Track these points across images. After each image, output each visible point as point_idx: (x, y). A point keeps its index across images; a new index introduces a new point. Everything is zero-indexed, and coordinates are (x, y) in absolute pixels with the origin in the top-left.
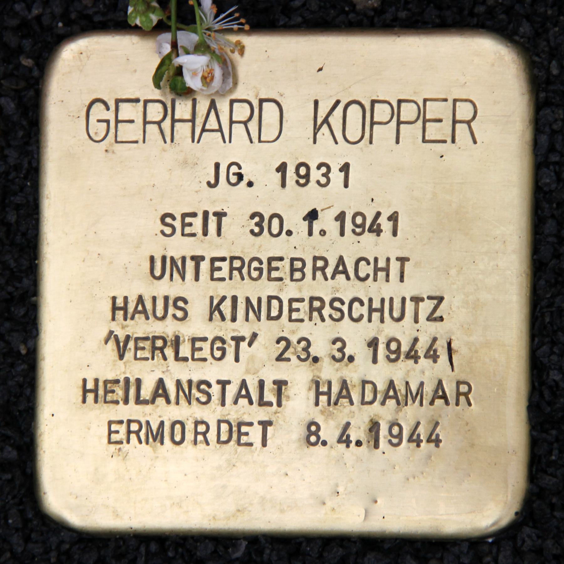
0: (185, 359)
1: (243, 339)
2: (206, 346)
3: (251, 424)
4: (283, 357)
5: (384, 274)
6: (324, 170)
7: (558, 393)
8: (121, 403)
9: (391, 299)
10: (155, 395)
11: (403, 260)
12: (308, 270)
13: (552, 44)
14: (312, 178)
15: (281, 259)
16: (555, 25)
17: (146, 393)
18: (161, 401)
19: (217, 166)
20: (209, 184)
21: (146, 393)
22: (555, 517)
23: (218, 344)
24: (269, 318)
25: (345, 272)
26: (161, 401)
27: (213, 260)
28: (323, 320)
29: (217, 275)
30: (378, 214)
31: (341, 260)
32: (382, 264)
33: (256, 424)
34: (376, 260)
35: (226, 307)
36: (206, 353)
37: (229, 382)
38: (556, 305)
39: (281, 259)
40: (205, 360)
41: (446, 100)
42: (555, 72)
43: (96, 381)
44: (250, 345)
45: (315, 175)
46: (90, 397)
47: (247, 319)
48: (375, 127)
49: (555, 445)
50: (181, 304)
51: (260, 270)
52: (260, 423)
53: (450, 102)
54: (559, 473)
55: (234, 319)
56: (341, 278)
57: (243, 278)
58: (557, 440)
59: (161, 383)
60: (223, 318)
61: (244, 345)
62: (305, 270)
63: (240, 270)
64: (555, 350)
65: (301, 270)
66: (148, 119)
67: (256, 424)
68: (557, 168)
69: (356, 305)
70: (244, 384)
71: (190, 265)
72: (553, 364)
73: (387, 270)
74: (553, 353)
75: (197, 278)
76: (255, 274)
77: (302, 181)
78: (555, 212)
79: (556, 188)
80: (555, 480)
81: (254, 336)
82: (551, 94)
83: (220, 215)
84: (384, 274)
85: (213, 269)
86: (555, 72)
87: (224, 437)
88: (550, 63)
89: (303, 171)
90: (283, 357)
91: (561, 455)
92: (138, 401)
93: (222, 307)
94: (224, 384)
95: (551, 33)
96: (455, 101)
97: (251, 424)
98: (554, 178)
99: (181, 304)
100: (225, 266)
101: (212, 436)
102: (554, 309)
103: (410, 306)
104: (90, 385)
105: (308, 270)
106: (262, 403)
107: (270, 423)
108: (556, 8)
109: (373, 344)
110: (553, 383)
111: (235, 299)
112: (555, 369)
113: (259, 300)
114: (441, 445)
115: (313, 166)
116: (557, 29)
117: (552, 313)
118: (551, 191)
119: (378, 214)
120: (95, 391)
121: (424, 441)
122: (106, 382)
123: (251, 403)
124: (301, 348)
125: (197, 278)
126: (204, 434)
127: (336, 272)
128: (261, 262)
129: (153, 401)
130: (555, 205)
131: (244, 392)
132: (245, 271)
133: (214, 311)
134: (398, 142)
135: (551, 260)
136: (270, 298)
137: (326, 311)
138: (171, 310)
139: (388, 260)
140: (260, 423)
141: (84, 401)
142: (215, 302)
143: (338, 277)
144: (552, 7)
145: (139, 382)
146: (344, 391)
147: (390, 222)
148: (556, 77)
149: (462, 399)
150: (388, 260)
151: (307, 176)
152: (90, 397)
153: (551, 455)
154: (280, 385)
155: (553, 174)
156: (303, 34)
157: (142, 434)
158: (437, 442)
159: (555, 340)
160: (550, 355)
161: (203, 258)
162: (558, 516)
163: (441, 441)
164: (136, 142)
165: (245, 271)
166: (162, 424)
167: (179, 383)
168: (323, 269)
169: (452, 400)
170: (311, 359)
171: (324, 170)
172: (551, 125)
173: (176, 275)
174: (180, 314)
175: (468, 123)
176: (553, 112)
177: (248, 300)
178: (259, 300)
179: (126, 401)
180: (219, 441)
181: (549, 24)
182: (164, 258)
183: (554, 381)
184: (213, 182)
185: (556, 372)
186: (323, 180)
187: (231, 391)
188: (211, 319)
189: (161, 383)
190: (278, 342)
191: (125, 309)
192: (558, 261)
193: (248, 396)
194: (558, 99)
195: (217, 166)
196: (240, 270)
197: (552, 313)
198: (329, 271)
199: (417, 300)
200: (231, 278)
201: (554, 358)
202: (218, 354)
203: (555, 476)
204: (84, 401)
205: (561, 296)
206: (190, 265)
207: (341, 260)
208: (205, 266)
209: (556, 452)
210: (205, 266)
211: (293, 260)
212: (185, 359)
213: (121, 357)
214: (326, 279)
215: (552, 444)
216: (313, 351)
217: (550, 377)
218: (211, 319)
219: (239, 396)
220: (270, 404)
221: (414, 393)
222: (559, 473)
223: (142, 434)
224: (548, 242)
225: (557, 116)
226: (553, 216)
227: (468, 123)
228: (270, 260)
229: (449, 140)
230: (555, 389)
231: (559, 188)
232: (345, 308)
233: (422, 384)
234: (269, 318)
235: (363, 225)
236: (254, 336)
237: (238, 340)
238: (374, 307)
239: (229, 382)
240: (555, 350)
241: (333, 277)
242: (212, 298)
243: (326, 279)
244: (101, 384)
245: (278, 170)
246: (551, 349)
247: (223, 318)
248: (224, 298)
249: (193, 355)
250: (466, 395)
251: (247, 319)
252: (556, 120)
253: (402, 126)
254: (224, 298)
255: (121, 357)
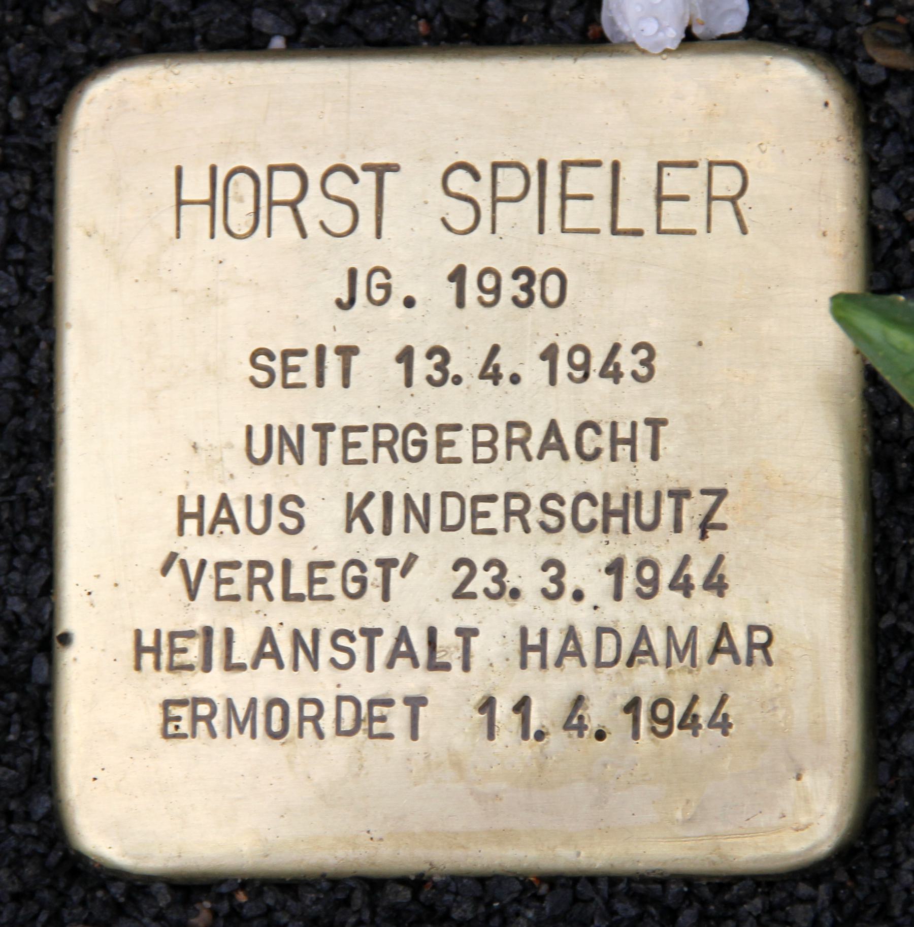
0: (299, 598)
1: (394, 562)
2: (334, 575)
3: (389, 703)
4: (465, 591)
5: (628, 448)
6: (643, 354)
7: (21, 632)
8: (198, 669)
9: (638, 495)
10: (260, 655)
11: (656, 424)
12: (501, 444)
13: (14, 70)
14: (503, 292)
15: (457, 427)
16: (19, 40)
17: (243, 652)
18: (267, 664)
19: (353, 274)
20: (339, 303)
21: (243, 652)
22: (12, 833)
23: (354, 571)
24: (445, 527)
25: (560, 446)
26: (267, 664)
27: (347, 430)
28: (527, 530)
29: (353, 454)
30: (616, 348)
31: (553, 428)
32: (624, 432)
33: (399, 702)
34: (614, 425)
35: (374, 511)
36: (333, 586)
37: (379, 632)
38: (19, 491)
39: (457, 427)
40: (330, 598)
41: (692, 165)
42: (17, 114)
43: (158, 633)
44: (404, 573)
45: (511, 288)
46: (148, 659)
47: (407, 530)
48: (500, 206)
49: (16, 717)
50: (291, 506)
51: (422, 444)
52: (407, 700)
53: (703, 166)
54: (20, 761)
55: (387, 531)
56: (552, 456)
57: (395, 459)
58: (18, 709)
59: (268, 636)
60: (369, 529)
61: (395, 572)
62: (497, 444)
63: (389, 445)
64: (17, 563)
65: (491, 444)
66: (499, 194)
67: (399, 702)
68: (20, 270)
69: (584, 504)
70: (403, 635)
71: (312, 440)
72: (14, 587)
73: (631, 442)
74: (12, 568)
75: (323, 461)
76: (414, 451)
77: (489, 298)
78: (17, 342)
79: (19, 303)
80: (13, 772)
81: (412, 559)
82: (10, 151)
83: (347, 352)
84: (628, 448)
85: (347, 446)
86: (17, 114)
87: (347, 725)
88: (8, 100)
89: (489, 282)
90: (465, 591)
91: (24, 733)
92: (230, 666)
93: (367, 510)
94: (371, 634)
95: (11, 52)
96: (711, 164)
97: (389, 703)
98: (15, 286)
99: (291, 506)
100: (366, 439)
101: (327, 723)
102: (13, 498)
103: (668, 505)
104: (148, 640)
105: (501, 444)
106: (434, 665)
107: (422, 701)
108: (19, 12)
109: (615, 568)
110: (12, 618)
111: (388, 498)
112: (16, 594)
113: (427, 498)
114: (731, 731)
115: (506, 275)
116: (20, 46)
117: (11, 503)
118: (11, 308)
119: (616, 348)
120: (156, 650)
121: (704, 726)
122: (173, 635)
123: (416, 664)
124: (157, 570)
125: (323, 461)
126: (315, 719)
127: (545, 447)
128: (423, 432)
129: (255, 665)
130: (17, 331)
131: (268, 648)
132: (398, 447)
133: (353, 519)
134: (744, 231)
135: (10, 419)
136: (445, 495)
137: (534, 516)
138: (277, 516)
139: (634, 425)
140: (407, 700)
141: (138, 667)
142: (357, 501)
143: (548, 454)
144: (14, 9)
145: (229, 634)
146: (571, 643)
147: (400, 365)
148: (20, 122)
149: (516, 449)
150: (634, 425)
151: (497, 290)
152: (148, 659)
153: (8, 733)
154: (466, 634)
155: (13, 280)
156: (548, 54)
157: (218, 722)
158: (725, 726)
159: (16, 547)
160: (9, 572)
161: (331, 427)
162: (17, 832)
163: (730, 725)
164: (692, 232)
165: (398, 447)
166: (253, 702)
167: (297, 636)
168: (522, 443)
169: (743, 652)
170: (507, 594)
171: (643, 354)
172: (8, 201)
173: (288, 456)
174: (291, 523)
175: (733, 200)
176: (13, 179)
177: (408, 498)
178: (427, 498)
179: (207, 666)
180: (339, 732)
181: (8, 37)
182: (269, 429)
183: (14, 613)
184: (345, 299)
185: (16, 599)
186: (643, 371)
187: (383, 647)
188: (349, 529)
189: (268, 636)
190: (456, 568)
191: (199, 515)
192: (22, 420)
193: (411, 654)
194: (21, 158)
195: (353, 274)
196: (389, 445)
197: (11, 503)
198: (534, 446)
199: (680, 495)
200: (375, 460)
201: (15, 577)
202: (353, 588)
203: (12, 766)
204: (138, 667)
205: (25, 478)
206: (312, 440)
207: (553, 428)
208: (334, 438)
209: (15, 728)
210: (334, 438)
211: (476, 428)
212: (299, 598)
213: (192, 595)
214: (529, 458)
215: (9, 715)
216: (511, 581)
217: (9, 607)
218: (349, 529)
219: (395, 654)
220: (446, 667)
221: (681, 646)
222: (20, 761)
223: (218, 722)
224: (6, 389)
225: (19, 186)
226: (13, 348)
227: (733, 200)
228: (440, 429)
229: (700, 227)
230: (15, 627)
231: (23, 302)
232: (566, 511)
233: (694, 630)
234: (445, 527)
235: (669, 721)
236: (412, 559)
237: (386, 564)
238: (612, 507)
239: (379, 632)
240: (17, 563)
241: (540, 456)
242: (350, 496)
243: (529, 458)
244: (164, 639)
245: (451, 278)
246: (10, 562)
247: (369, 529)
248: (370, 496)
249: (311, 590)
250: (764, 647)
251: (407, 530)
252: (18, 193)
253: (714, 203)
254: (370, 496)
255: (192, 595)
